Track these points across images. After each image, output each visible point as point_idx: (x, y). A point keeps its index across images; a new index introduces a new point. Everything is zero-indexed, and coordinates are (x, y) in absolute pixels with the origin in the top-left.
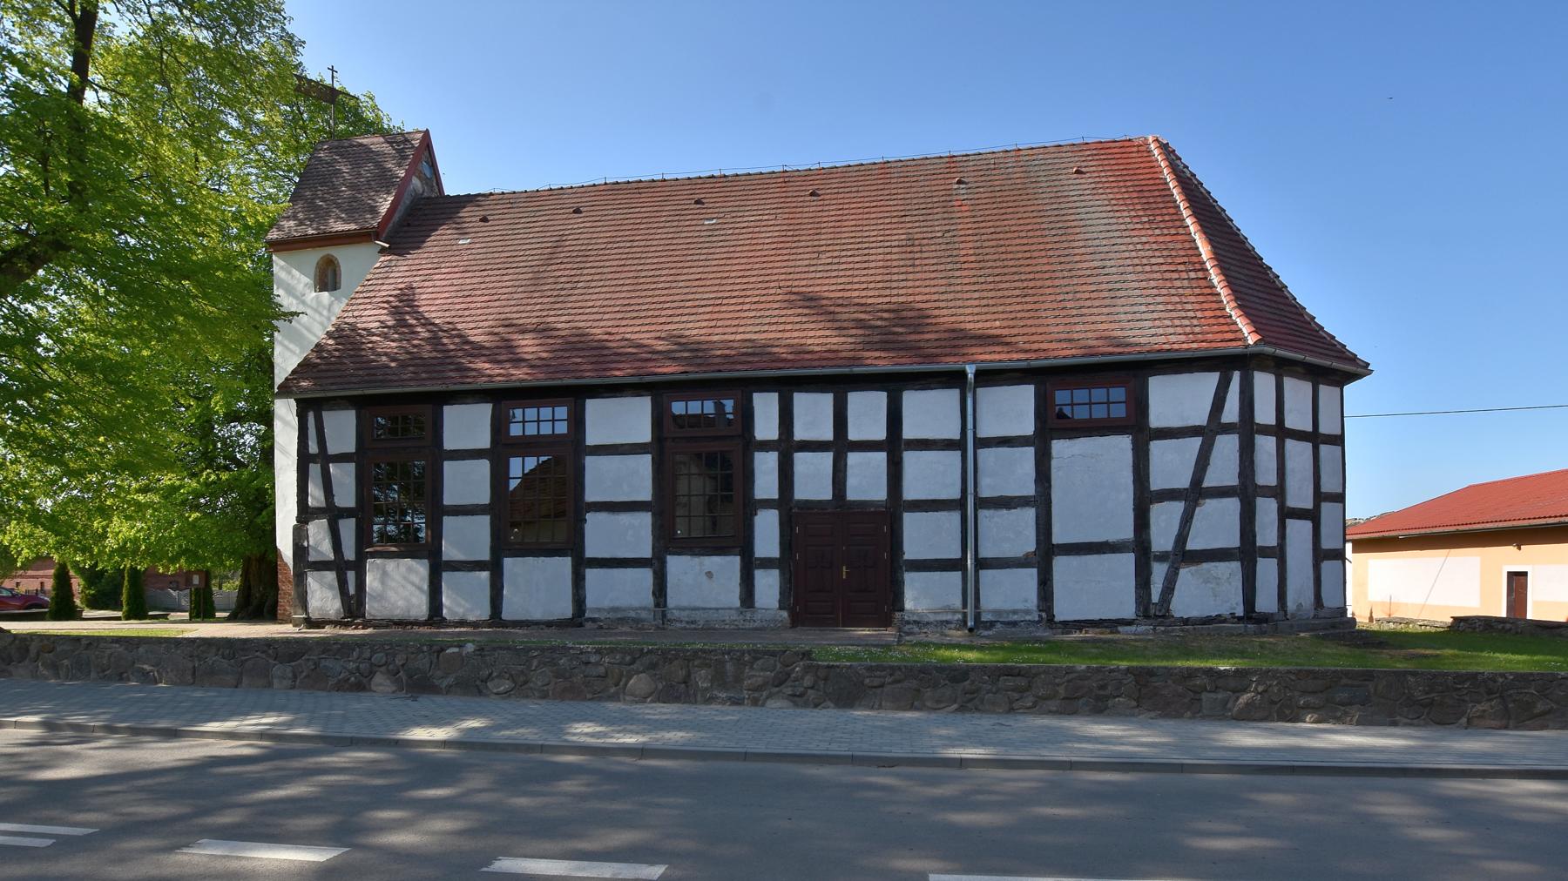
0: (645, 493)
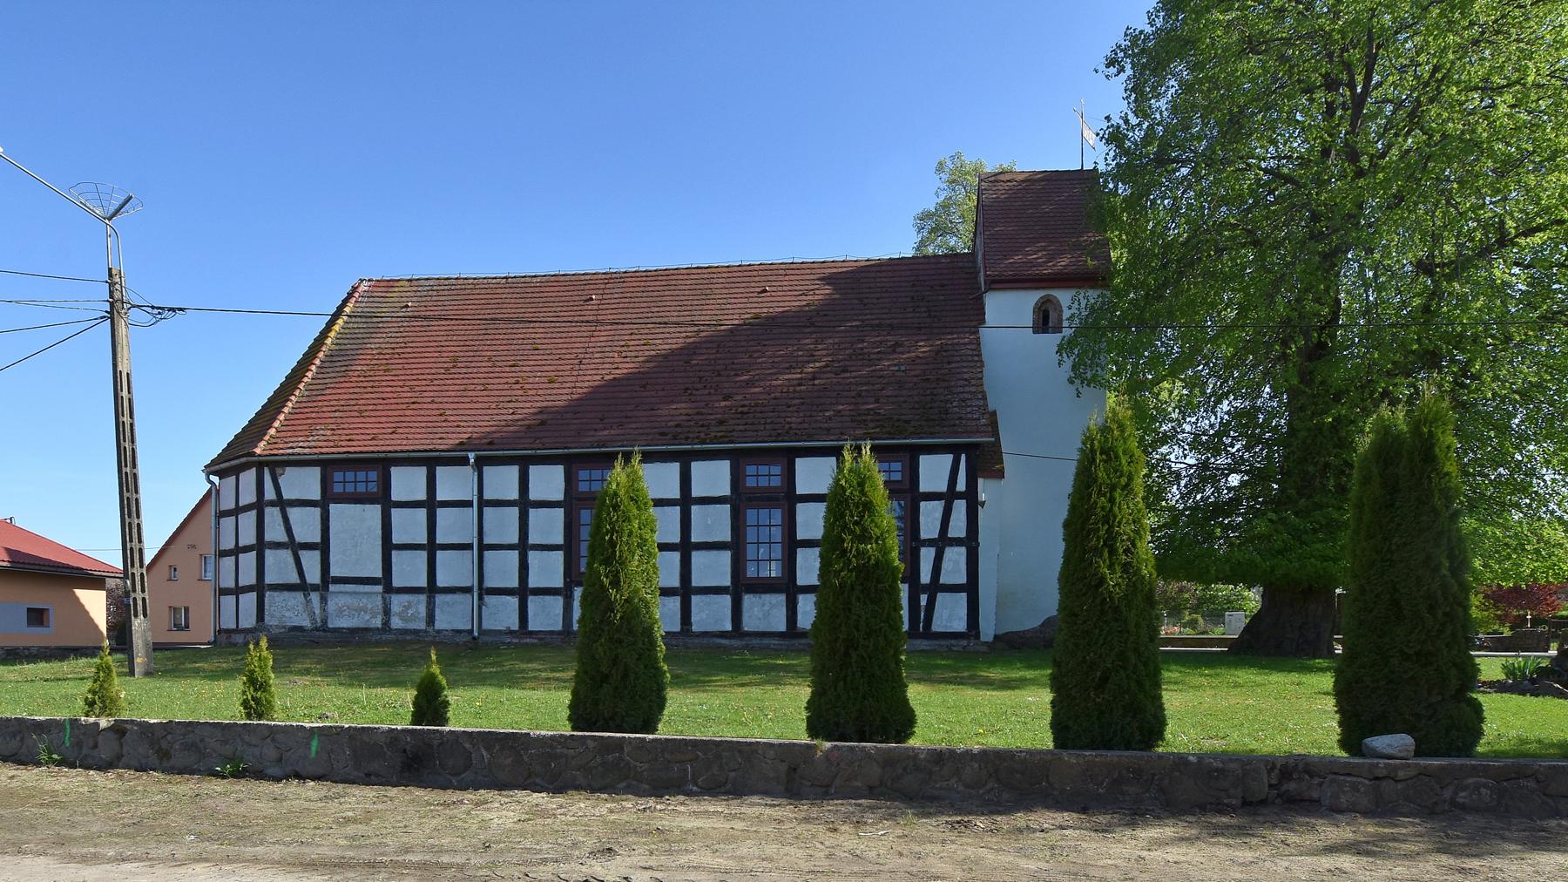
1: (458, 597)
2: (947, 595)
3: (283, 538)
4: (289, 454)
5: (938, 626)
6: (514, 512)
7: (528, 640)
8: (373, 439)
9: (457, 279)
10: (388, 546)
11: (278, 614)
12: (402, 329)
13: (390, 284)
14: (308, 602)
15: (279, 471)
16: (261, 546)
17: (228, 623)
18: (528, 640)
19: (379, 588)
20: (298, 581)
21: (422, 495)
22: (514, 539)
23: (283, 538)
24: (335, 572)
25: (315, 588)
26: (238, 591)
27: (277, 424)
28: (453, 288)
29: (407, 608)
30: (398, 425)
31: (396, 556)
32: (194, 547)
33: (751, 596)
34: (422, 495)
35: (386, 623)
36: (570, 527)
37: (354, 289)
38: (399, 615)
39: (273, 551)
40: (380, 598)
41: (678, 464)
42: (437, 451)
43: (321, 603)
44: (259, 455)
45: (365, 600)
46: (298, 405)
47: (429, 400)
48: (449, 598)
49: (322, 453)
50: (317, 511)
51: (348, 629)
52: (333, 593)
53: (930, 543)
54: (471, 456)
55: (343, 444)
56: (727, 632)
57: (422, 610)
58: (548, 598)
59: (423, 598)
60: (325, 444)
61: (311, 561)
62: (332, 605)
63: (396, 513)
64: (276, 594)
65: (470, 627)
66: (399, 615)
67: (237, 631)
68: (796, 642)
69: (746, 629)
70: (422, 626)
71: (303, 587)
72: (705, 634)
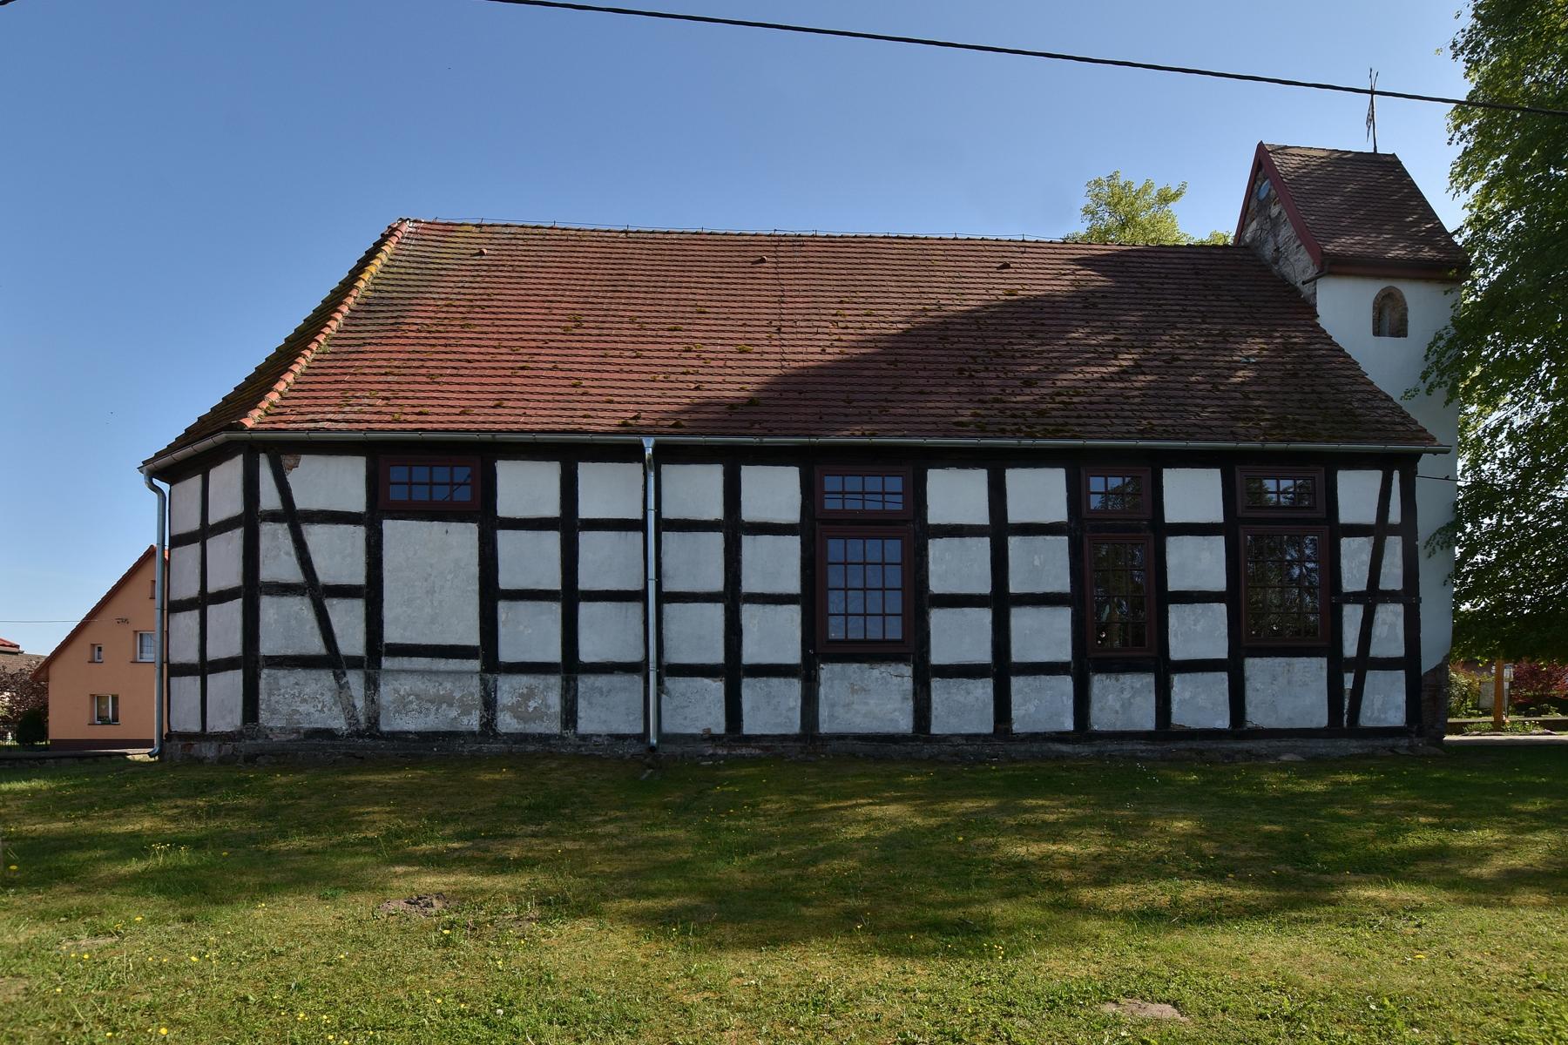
0: (1219, 583)
1: (617, 680)
2: (1380, 674)
3: (294, 575)
4: (309, 430)
5: (1367, 719)
6: (717, 540)
7: (744, 751)
8: (461, 414)
9: (551, 228)
10: (491, 593)
11: (284, 709)
12: (479, 279)
13: (449, 228)
14: (341, 687)
15: (287, 460)
16: (251, 590)
17: (186, 719)
18: (744, 751)
19: (475, 665)
20: (324, 651)
21: (552, 509)
22: (717, 583)
23: (294, 575)
24: (392, 635)
25: (354, 663)
26: (204, 668)
27: (281, 386)
28: (548, 237)
29: (530, 695)
30: (504, 396)
31: (504, 609)
32: (126, 621)
33: (1104, 677)
34: (552, 509)
35: (489, 723)
36: (811, 566)
37: (392, 231)
38: (513, 709)
39: (275, 599)
40: (476, 681)
41: (984, 472)
42: (586, 432)
43: (367, 688)
44: (252, 430)
45: (449, 685)
46: (316, 364)
47: (550, 366)
48: (602, 681)
49: (372, 430)
50: (359, 532)
51: (418, 733)
52: (388, 671)
53: (1355, 597)
54: (649, 444)
55: (409, 418)
56: (1068, 733)
57: (555, 700)
58: (775, 682)
59: (555, 681)
60: (376, 417)
61: (348, 621)
62: (388, 692)
63: (505, 538)
64: (281, 673)
65: (640, 730)
66: (513, 709)
67: (203, 736)
68: (1171, 746)
69: (1096, 727)
70: (554, 727)
71: (332, 660)
72: (1034, 737)
